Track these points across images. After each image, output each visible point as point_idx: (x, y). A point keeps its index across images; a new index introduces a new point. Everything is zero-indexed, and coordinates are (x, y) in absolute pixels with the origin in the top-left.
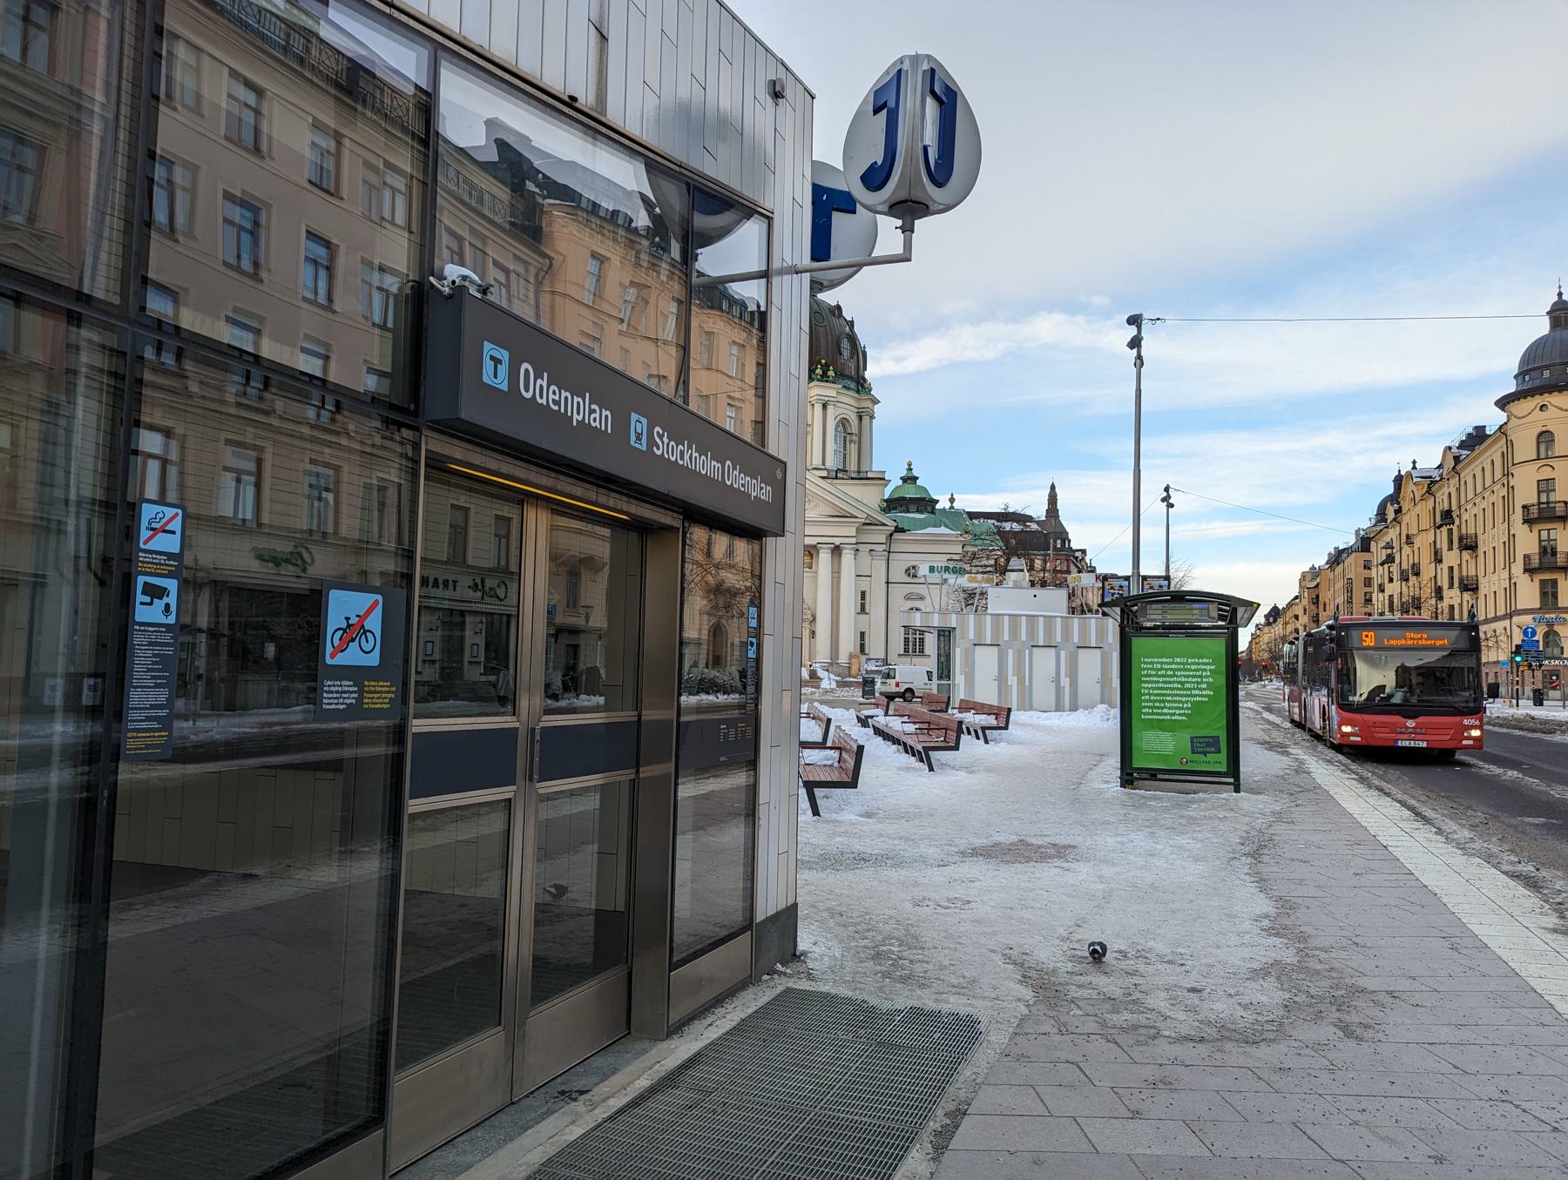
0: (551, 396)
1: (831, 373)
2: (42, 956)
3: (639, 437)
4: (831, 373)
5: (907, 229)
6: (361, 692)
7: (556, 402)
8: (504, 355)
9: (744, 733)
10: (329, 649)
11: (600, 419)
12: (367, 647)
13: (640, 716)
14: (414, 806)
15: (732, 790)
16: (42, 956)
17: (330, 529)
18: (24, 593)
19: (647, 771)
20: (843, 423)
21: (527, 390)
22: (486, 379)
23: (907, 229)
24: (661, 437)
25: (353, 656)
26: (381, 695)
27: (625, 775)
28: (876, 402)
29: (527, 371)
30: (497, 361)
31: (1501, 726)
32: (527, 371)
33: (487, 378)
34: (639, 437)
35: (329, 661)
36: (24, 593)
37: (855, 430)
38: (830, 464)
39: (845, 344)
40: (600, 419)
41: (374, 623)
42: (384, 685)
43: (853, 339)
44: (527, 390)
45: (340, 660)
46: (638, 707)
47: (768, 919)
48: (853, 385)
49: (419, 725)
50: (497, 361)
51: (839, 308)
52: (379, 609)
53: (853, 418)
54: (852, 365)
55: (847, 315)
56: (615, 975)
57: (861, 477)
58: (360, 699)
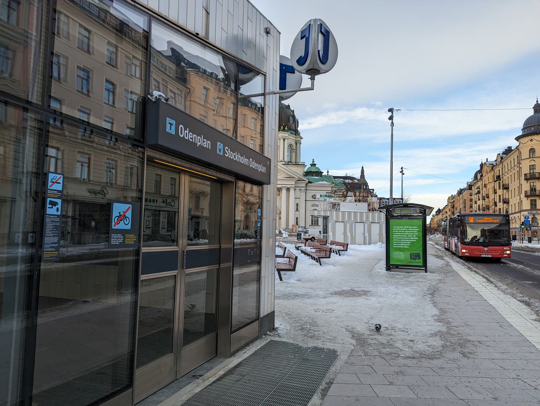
0: (190, 136)
1: (286, 128)
2: (14, 329)
3: (220, 150)
4: (286, 128)
5: (313, 79)
6: (124, 238)
7: (191, 138)
8: (173, 122)
9: (256, 252)
10: (113, 223)
11: (207, 144)
12: (126, 223)
13: (220, 246)
14: (143, 277)
16: (14, 329)
18: (8, 204)
19: (223, 265)
20: (290, 145)
21: (181, 134)
22: (167, 130)
23: (313, 79)
25: (121, 226)
26: (131, 239)
27: (215, 267)
28: (302, 138)
29: (181, 128)
30: (171, 124)
31: (517, 250)
32: (181, 128)
33: (168, 130)
34: (220, 150)
35: (113, 227)
36: (8, 204)
37: (294, 148)
38: (286, 159)
39: (291, 118)
40: (207, 144)
41: (129, 214)
42: (132, 236)
43: (294, 117)
44: (181, 134)
45: (117, 227)
46: (220, 243)
47: (265, 316)
48: (294, 132)
50: (171, 124)
51: (289, 106)
52: (131, 209)
53: (294, 144)
54: (294, 126)
55: (292, 108)
57: (297, 164)
58: (124, 241)
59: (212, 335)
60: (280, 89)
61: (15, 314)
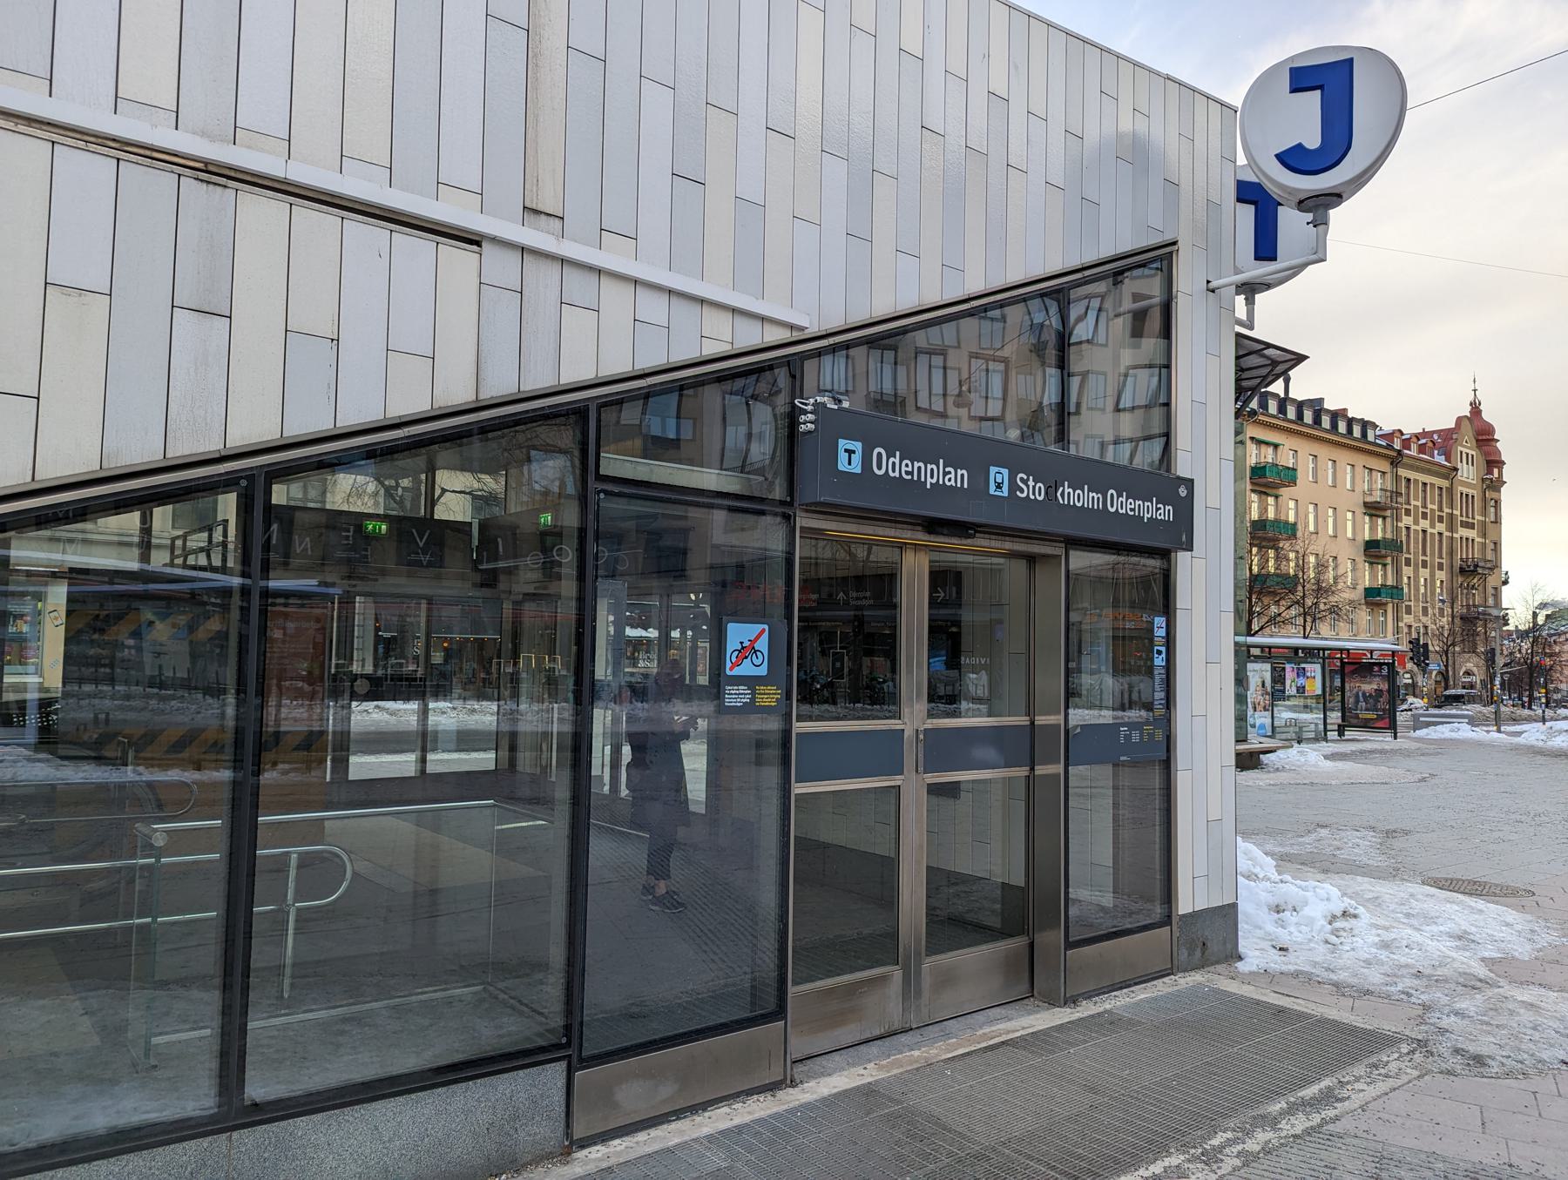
0: (904, 469)
2: (289, 961)
3: (999, 486)
6: (754, 694)
7: (911, 473)
8: (857, 446)
9: (1152, 736)
10: (728, 665)
11: (957, 478)
12: (757, 662)
13: (1032, 723)
14: (799, 789)
16: (289, 961)
19: (1040, 770)
21: (879, 468)
22: (841, 467)
24: (1025, 482)
25: (746, 669)
26: (770, 696)
27: (1022, 772)
29: (879, 454)
30: (850, 452)
32: (879, 454)
33: (842, 465)
34: (999, 486)
35: (728, 673)
40: (957, 478)
41: (763, 645)
42: (772, 689)
44: (879, 468)
45: (737, 671)
46: (1030, 711)
47: (1194, 915)
50: (850, 452)
52: (766, 634)
56: (1018, 943)
58: (753, 699)
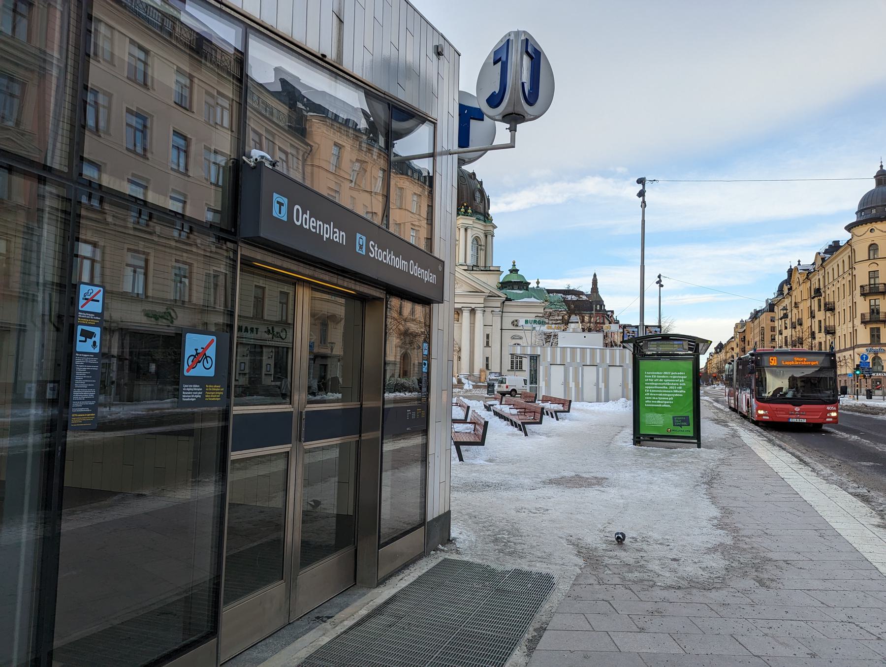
0: (311, 224)
1: (470, 211)
3: (361, 247)
4: (470, 211)
5: (513, 129)
6: (204, 391)
7: (314, 227)
8: (285, 201)
9: (420, 414)
10: (186, 367)
11: (339, 237)
12: (207, 366)
13: (361, 405)
14: (234, 455)
15: (414, 447)
17: (187, 299)
18: (14, 335)
19: (365, 436)
20: (477, 239)
21: (298, 221)
22: (274, 214)
23: (513, 129)
24: (373, 247)
25: (199, 371)
26: (215, 393)
27: (353, 438)
28: (495, 227)
29: (298, 210)
30: (281, 204)
32: (298, 210)
33: (275, 213)
34: (361, 247)
35: (186, 374)
36: (14, 335)
37: (483, 243)
38: (469, 262)
39: (478, 195)
40: (339, 237)
41: (211, 352)
42: (217, 387)
43: (482, 192)
44: (298, 221)
45: (192, 373)
46: (360, 399)
47: (434, 520)
48: (482, 218)
49: (237, 410)
50: (281, 204)
51: (474, 174)
52: (214, 344)
53: (482, 236)
54: (482, 206)
55: (479, 178)
57: (487, 270)
58: (203, 395)
59: (347, 551)
60: (460, 146)
61: (25, 517)
